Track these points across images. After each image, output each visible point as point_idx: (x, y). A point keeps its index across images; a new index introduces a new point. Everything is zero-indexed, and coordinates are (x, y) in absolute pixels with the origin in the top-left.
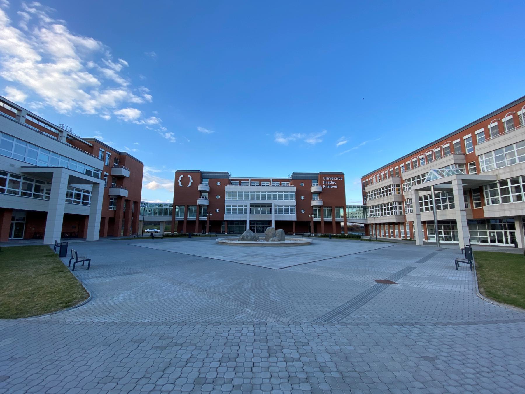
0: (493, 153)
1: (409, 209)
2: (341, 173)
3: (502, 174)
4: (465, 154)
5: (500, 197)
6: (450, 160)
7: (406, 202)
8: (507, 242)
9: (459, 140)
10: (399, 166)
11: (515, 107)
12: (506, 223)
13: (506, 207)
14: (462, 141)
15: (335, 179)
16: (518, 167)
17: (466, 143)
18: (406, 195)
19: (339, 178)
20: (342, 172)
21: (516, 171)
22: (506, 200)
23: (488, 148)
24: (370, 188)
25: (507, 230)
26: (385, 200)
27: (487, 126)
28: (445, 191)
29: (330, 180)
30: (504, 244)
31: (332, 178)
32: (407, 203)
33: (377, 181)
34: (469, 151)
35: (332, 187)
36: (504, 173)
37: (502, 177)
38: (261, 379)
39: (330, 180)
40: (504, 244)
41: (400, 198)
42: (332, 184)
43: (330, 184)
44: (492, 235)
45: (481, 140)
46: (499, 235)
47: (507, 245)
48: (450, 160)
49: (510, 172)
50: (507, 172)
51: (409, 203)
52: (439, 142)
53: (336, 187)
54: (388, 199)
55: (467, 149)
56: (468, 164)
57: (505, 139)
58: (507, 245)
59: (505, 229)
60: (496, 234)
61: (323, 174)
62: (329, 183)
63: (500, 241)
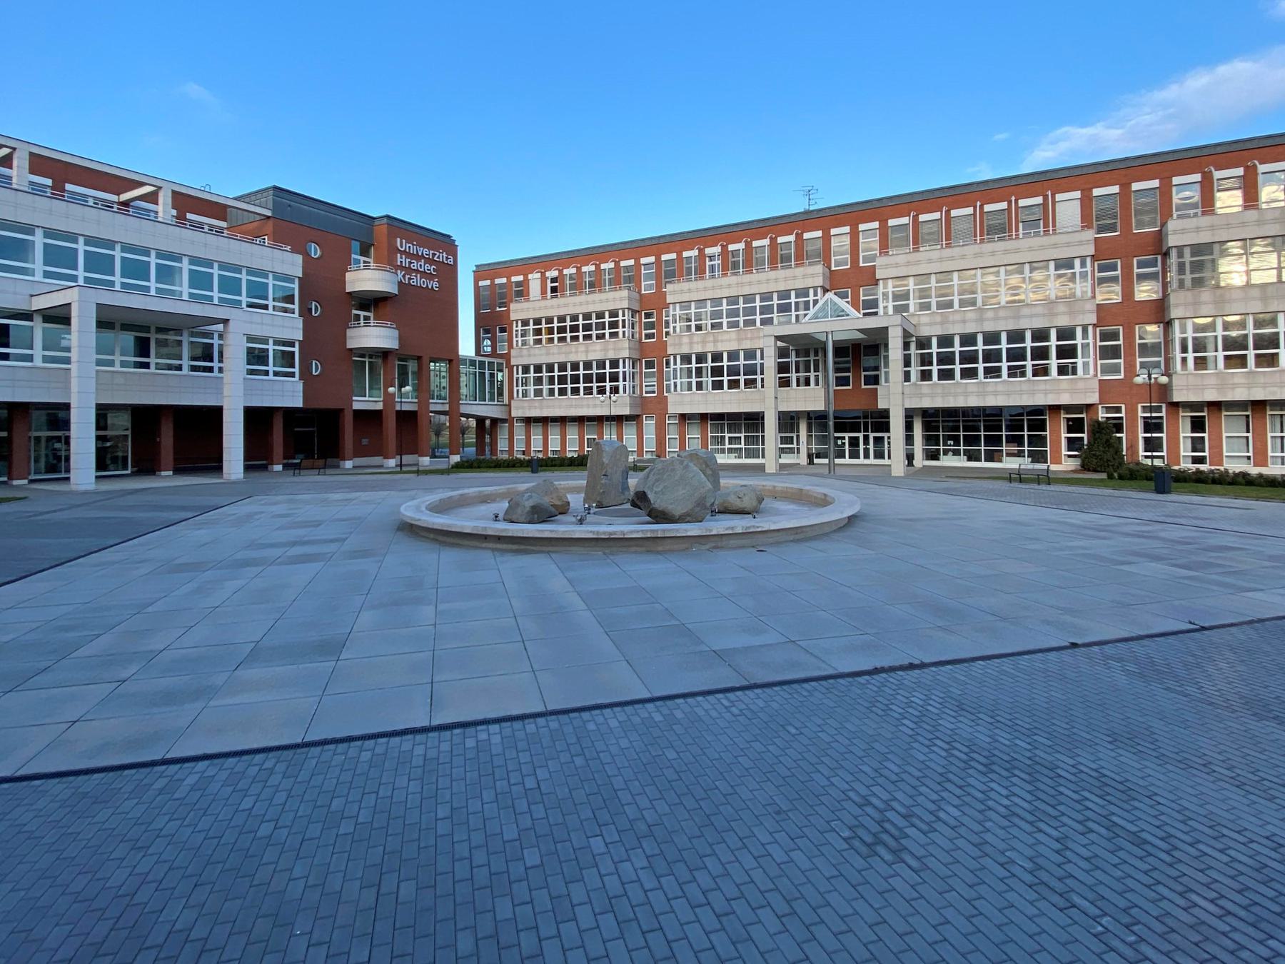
0: (709, 302)
1: (520, 388)
2: (446, 240)
3: (926, 324)
4: (639, 292)
5: (1054, 363)
6: (813, 276)
7: (668, 363)
8: (867, 456)
9: (631, 262)
10: (509, 278)
11: (950, 199)
12: (1025, 418)
13: (1064, 386)
14: (638, 264)
15: (434, 255)
16: (957, 317)
17: (643, 272)
18: (674, 345)
19: (445, 255)
20: (449, 237)
21: (954, 322)
22: (1041, 371)
23: (938, 264)
24: (534, 309)
25: (862, 433)
26: (988, 319)
27: (886, 221)
28: (792, 346)
29: (418, 257)
30: (862, 461)
31: (426, 251)
32: (672, 366)
33: (544, 292)
34: (866, 259)
35: (424, 283)
36: (930, 324)
37: (925, 332)
38: (417, 940)
39: (418, 257)
40: (862, 461)
41: (635, 349)
42: (424, 274)
43: (417, 271)
44: (839, 442)
45: (903, 243)
46: (854, 442)
47: (867, 462)
48: (813, 276)
49: (942, 323)
50: (935, 324)
51: (520, 375)
52: (597, 254)
53: (435, 285)
54: (704, 342)
55: (643, 284)
56: (643, 313)
57: (1198, 228)
58: (867, 462)
59: (866, 430)
60: (847, 441)
61: (397, 226)
62: (415, 266)
63: (854, 455)
